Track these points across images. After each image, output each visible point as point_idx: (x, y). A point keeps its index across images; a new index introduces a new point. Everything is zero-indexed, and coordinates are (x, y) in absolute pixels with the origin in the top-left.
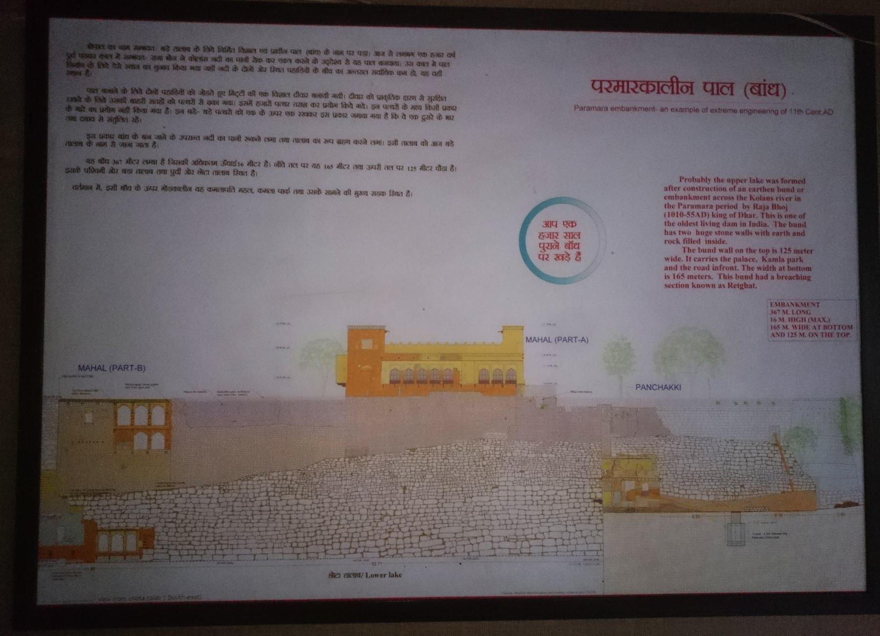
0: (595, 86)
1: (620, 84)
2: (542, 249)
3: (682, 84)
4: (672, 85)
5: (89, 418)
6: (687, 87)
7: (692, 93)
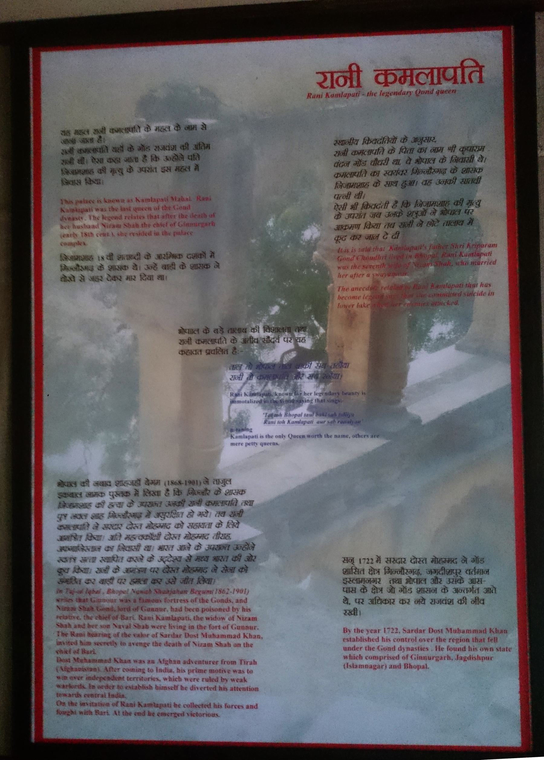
0: (393, 80)
1: (408, 73)
2: (111, 497)
3: (339, 74)
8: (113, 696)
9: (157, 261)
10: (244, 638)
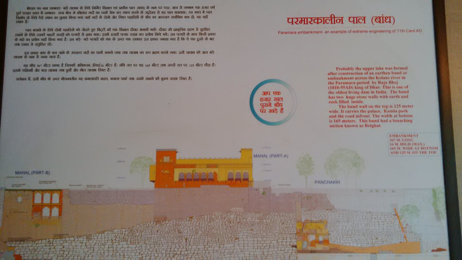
0: (321, 21)
1: (303, 19)
4: (331, 19)
5: (20, 199)
6: (340, 20)
7: (342, 23)
8: (379, 92)
9: (90, 15)
10: (377, 79)
